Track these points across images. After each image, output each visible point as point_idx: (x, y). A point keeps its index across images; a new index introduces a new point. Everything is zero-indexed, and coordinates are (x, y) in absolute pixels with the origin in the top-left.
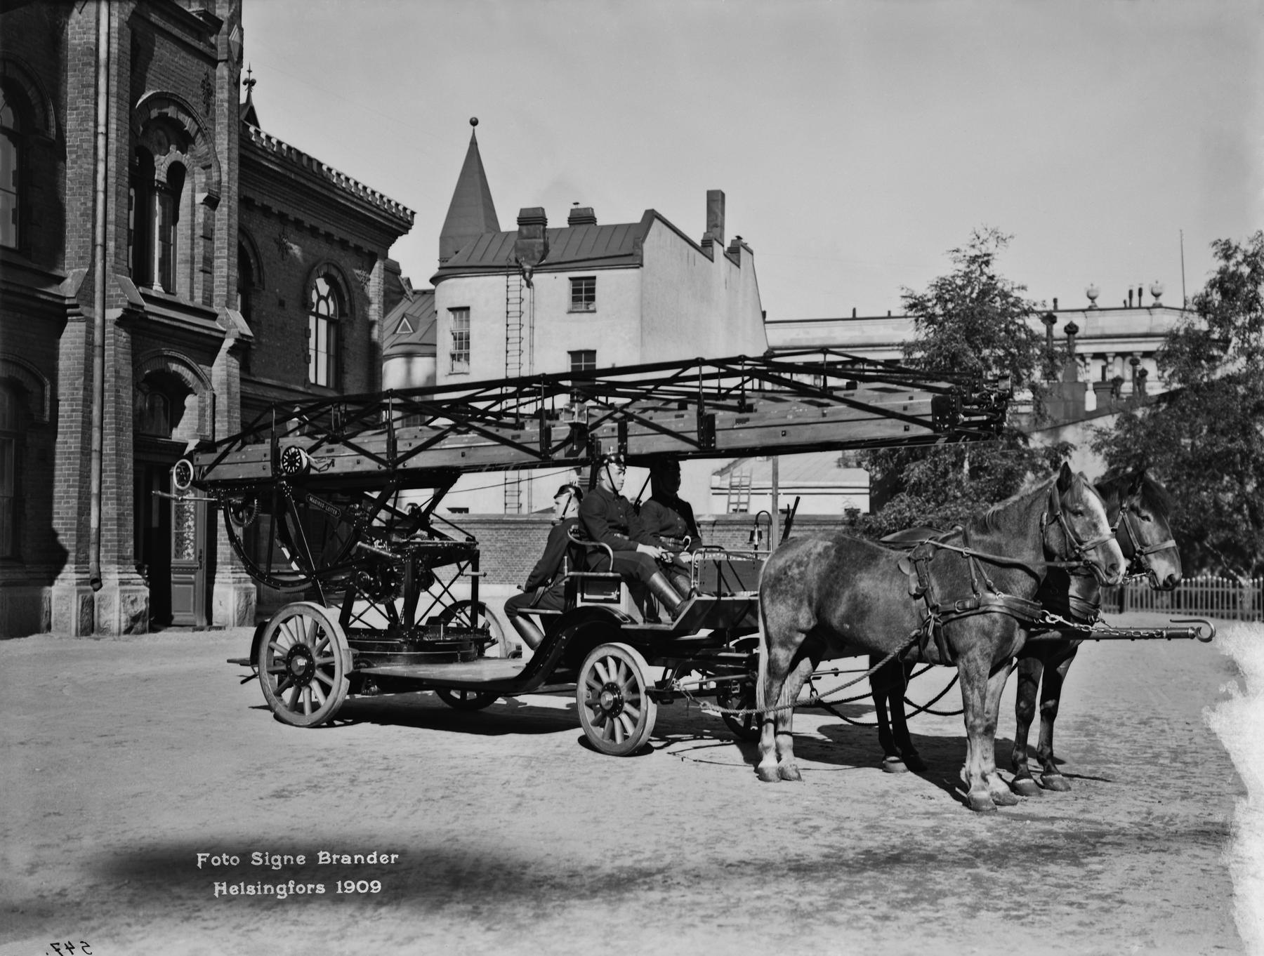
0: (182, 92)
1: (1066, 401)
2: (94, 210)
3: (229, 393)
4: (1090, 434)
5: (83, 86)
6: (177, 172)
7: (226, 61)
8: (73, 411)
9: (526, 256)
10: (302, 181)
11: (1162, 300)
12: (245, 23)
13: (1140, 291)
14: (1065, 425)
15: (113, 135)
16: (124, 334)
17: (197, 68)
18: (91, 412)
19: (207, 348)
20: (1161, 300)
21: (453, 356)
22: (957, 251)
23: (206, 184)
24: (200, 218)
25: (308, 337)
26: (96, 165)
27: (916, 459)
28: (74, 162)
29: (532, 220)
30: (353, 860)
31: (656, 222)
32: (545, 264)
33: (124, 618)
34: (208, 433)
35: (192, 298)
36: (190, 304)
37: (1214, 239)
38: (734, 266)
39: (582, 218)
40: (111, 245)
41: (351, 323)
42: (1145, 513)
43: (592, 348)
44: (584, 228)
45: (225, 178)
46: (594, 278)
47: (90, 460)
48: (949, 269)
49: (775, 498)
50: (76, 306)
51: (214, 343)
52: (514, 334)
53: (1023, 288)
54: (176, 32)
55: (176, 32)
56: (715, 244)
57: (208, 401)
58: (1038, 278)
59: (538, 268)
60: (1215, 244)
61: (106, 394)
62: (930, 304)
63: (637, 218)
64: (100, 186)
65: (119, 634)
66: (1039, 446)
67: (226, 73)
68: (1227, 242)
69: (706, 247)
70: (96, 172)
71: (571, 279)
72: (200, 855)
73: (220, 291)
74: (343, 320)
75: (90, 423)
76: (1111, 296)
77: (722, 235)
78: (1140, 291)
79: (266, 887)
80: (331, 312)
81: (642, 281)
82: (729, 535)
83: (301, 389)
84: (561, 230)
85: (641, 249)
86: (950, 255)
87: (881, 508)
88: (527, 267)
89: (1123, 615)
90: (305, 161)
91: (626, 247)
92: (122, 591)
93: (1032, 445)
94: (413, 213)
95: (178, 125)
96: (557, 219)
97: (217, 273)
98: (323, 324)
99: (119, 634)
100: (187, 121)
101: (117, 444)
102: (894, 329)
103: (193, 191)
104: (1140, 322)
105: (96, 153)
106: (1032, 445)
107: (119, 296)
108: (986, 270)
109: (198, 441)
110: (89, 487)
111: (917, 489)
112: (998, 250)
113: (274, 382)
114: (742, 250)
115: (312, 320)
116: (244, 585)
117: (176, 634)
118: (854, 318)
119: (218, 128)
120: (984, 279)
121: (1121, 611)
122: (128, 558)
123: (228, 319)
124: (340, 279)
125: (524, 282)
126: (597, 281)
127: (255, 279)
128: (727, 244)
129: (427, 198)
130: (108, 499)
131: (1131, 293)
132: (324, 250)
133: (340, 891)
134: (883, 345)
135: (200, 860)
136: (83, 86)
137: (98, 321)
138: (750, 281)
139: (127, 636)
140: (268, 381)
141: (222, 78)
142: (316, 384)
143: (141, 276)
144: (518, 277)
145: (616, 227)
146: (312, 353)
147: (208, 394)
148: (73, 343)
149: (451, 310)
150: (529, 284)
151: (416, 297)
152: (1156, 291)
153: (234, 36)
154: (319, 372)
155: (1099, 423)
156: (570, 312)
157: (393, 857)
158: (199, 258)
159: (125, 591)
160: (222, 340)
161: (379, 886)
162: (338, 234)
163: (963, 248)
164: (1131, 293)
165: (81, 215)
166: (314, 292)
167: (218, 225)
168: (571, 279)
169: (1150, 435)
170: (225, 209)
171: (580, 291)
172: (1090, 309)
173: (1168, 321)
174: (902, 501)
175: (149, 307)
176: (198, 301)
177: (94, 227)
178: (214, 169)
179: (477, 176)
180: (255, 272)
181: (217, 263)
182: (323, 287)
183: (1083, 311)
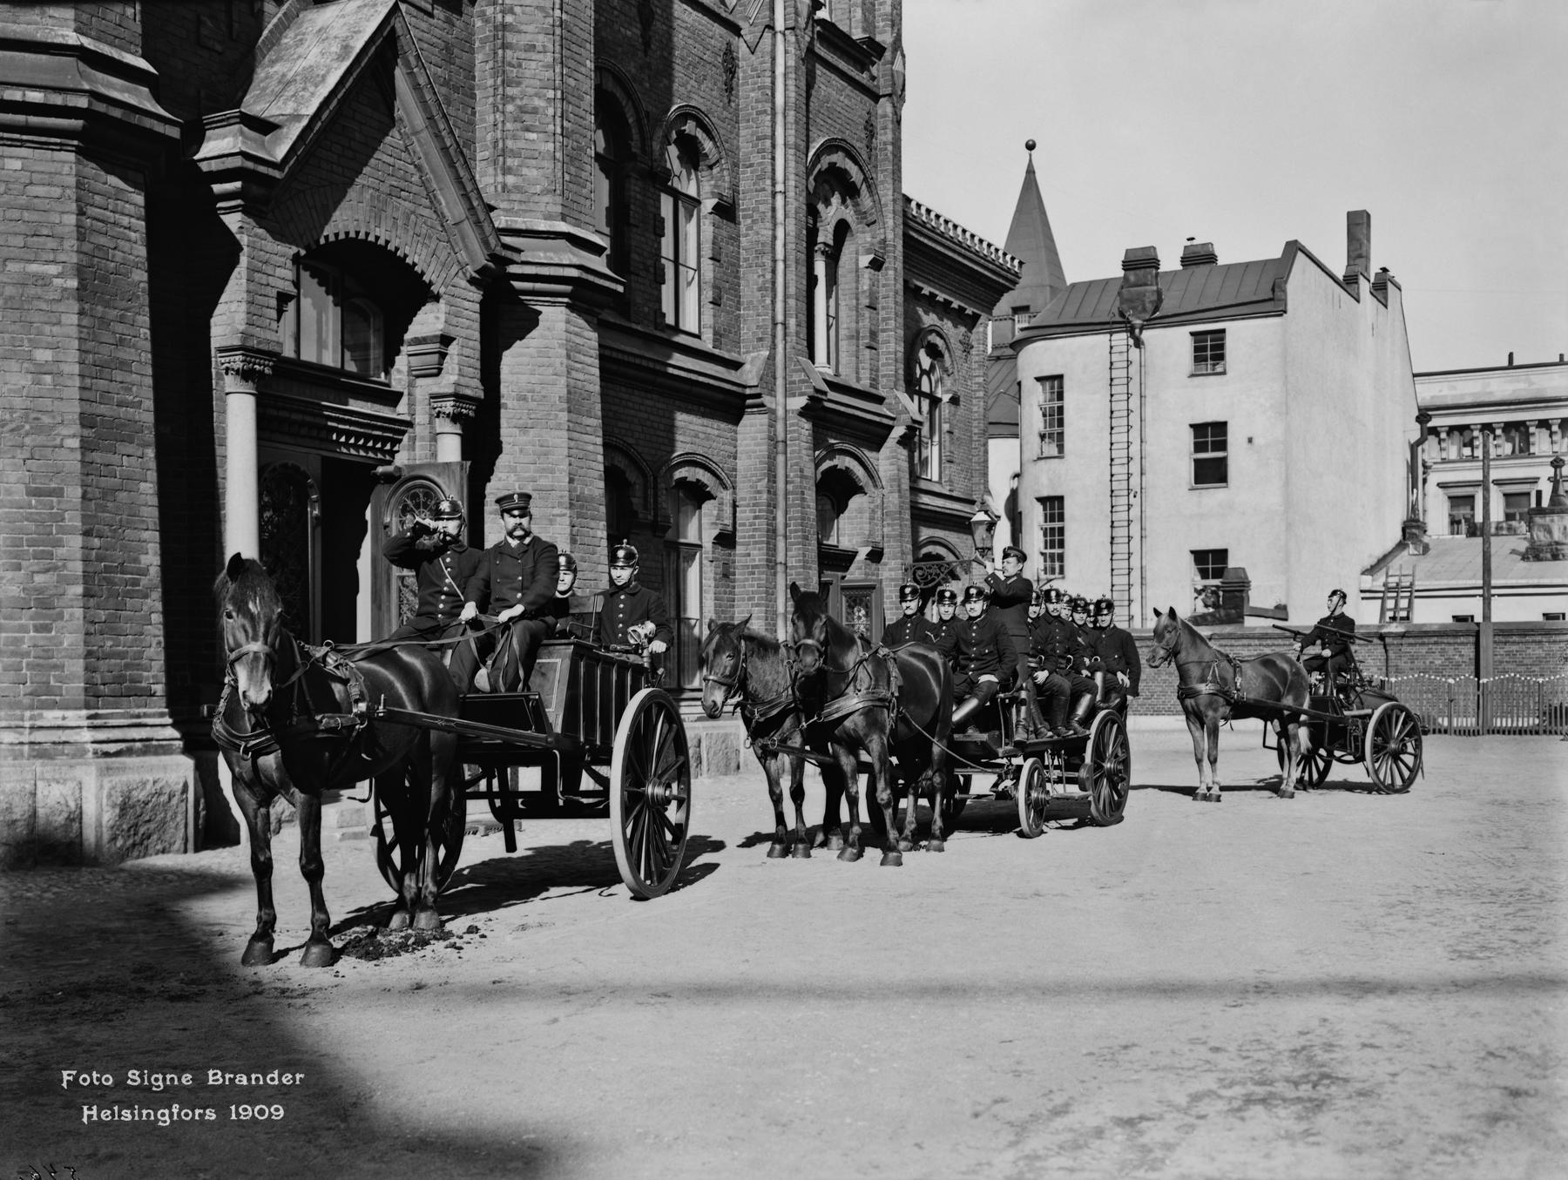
0: (847, 136)
2: (774, 283)
5: (758, 139)
6: (842, 229)
7: (890, 95)
8: (756, 518)
15: (791, 194)
17: (859, 102)
18: (775, 518)
21: (1042, 437)
26: (774, 230)
28: (750, 228)
29: (1140, 263)
30: (294, 1079)
35: (858, 379)
39: (1198, 258)
40: (792, 322)
43: (1221, 419)
44: (1204, 269)
45: (890, 236)
46: (1223, 331)
47: (775, 574)
50: (759, 396)
52: (1120, 406)
54: (842, 65)
55: (842, 65)
59: (1151, 323)
63: (1277, 253)
64: (780, 255)
67: (889, 109)
69: (1349, 282)
70: (774, 238)
71: (1192, 334)
72: (65, 1073)
75: (774, 531)
77: (1367, 268)
79: (145, 1112)
82: (1424, 650)
84: (1176, 272)
85: (1284, 291)
88: (1138, 322)
91: (1265, 290)
95: (844, 173)
96: (1170, 261)
97: (883, 349)
105: (774, 217)
110: (775, 606)
114: (1390, 285)
118: (1511, 366)
119: (881, 177)
125: (1131, 342)
133: (234, 1117)
135: (66, 1078)
136: (758, 139)
137: (780, 412)
138: (1399, 324)
141: (885, 116)
144: (1124, 335)
145: (1248, 265)
148: (754, 439)
149: (1038, 379)
150: (1138, 343)
156: (1192, 376)
157: (298, 1076)
158: (865, 333)
160: (891, 428)
161: (282, 1112)
165: (760, 290)
168: (1192, 334)
177: (773, 302)
181: (882, 336)
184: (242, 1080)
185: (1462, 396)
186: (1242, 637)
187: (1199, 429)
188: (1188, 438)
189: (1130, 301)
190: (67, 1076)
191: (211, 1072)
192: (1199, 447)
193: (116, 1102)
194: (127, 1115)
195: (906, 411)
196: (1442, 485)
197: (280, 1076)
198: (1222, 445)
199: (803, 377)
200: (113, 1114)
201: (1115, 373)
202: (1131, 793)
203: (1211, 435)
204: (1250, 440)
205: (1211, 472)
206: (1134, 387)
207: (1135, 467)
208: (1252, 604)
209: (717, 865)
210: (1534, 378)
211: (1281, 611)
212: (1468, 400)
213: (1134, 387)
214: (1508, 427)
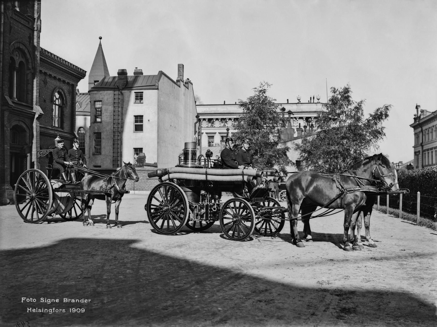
1: (288, 134)
4: (294, 146)
10: (52, 62)
12: (41, 18)
13: (314, 97)
20: (320, 101)
22: (256, 88)
29: (123, 73)
31: (163, 76)
38: (186, 89)
41: (66, 107)
42: (383, 166)
46: (143, 92)
48: (253, 94)
53: (275, 100)
63: (156, 73)
66: (280, 148)
68: (335, 89)
71: (135, 92)
72: (22, 298)
78: (314, 97)
83: (50, 128)
90: (53, 56)
91: (153, 83)
98: (57, 107)
104: (314, 107)
108: (264, 94)
114: (189, 83)
115: (54, 106)
118: (224, 104)
124: (62, 93)
126: (144, 93)
131: (311, 98)
132: (58, 84)
142: (55, 126)
145: (149, 76)
146: (54, 117)
150: (122, 94)
151: (81, 95)
152: (318, 98)
153: (39, 23)
155: (297, 141)
157: (89, 300)
160: (35, 115)
161: (84, 310)
162: (62, 78)
163: (257, 88)
164: (311, 98)
168: (135, 92)
172: (298, 103)
173: (319, 108)
182: (57, 96)
183: (296, 104)
184: (73, 301)
186: (143, 171)
187: (136, 117)
190: (23, 299)
192: (136, 121)
193: (54, 307)
194: (40, 311)
198: (142, 121)
202: (14, 206)
204: (149, 120)
205: (139, 128)
208: (146, 162)
209: (376, 246)
210: (228, 108)
211: (155, 165)
212: (213, 112)
214: (222, 119)
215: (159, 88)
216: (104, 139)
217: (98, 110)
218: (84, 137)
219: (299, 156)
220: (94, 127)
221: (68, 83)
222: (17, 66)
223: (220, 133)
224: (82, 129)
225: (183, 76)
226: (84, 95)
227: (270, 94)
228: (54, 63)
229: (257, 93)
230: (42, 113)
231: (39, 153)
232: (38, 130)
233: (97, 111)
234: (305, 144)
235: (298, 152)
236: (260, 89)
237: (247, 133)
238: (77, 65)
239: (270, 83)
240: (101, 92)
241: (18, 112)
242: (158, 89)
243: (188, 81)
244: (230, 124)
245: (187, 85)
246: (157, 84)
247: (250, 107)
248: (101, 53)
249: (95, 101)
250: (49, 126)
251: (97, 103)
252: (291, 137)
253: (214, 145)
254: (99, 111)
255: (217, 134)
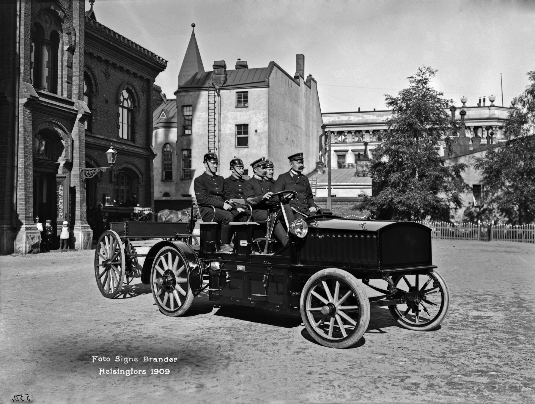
3: (79, 140)
4: (473, 161)
9: (217, 82)
10: (116, 45)
11: (495, 103)
13: (484, 99)
14: (461, 156)
16: (28, 111)
19: (69, 119)
20: (494, 103)
22: (412, 77)
23: (69, 41)
24: (66, 57)
25: (119, 117)
27: (394, 172)
29: (220, 66)
32: (225, 86)
33: (28, 246)
34: (70, 158)
35: (62, 95)
36: (61, 97)
37: (530, 71)
38: (308, 88)
39: (242, 66)
43: (246, 123)
45: (78, 39)
46: (247, 92)
48: (408, 85)
49: (330, 189)
51: (72, 116)
53: (442, 94)
56: (300, 78)
57: (70, 143)
58: (449, 89)
60: (529, 73)
61: (20, 139)
62: (399, 102)
63: (266, 65)
65: (26, 254)
71: (237, 92)
73: (75, 92)
74: (135, 109)
76: (472, 102)
78: (484, 99)
80: (129, 106)
81: (269, 93)
83: (115, 140)
84: (232, 71)
86: (408, 80)
87: (378, 194)
88: (217, 87)
89: (490, 242)
91: (262, 78)
92: (27, 233)
93: (446, 165)
94: (166, 62)
96: (231, 66)
97: (74, 83)
98: (126, 111)
99: (26, 254)
100: (60, 13)
101: (25, 163)
102: (377, 116)
103: (63, 44)
106: (446, 165)
107: (25, 92)
109: (65, 162)
111: (395, 185)
112: (430, 77)
113: (103, 137)
114: (312, 81)
115: (121, 109)
116: (87, 230)
117: (53, 253)
118: (359, 112)
119: (74, 16)
120: (424, 90)
121: (489, 240)
122: (30, 217)
123: (79, 105)
124: (133, 91)
125: (216, 94)
127: (94, 90)
128: (305, 78)
129: (172, 54)
130: (20, 189)
131: (480, 100)
134: (372, 123)
138: (315, 94)
139: (29, 255)
140: (100, 137)
142: (122, 138)
143: (38, 85)
144: (213, 92)
145: (257, 69)
146: (121, 124)
147: (70, 140)
151: (168, 102)
152: (492, 99)
154: (124, 133)
155: (478, 155)
156: (236, 107)
157: (175, 359)
159: (29, 233)
160: (76, 115)
161: (169, 371)
162: (132, 70)
164: (480, 100)
166: (122, 96)
167: (74, 61)
169: (502, 160)
170: (78, 53)
171: (241, 98)
174: (388, 190)
175: (41, 99)
176: (65, 96)
178: (72, 34)
179: (195, 50)
180: (94, 87)
181: (74, 78)
182: (126, 94)
184: (155, 360)
185: (342, 121)
187: (239, 126)
188: (234, 130)
189: (215, 80)
191: (145, 357)
192: (239, 133)
195: (82, 108)
196: (335, 151)
197: (169, 359)
198: (246, 133)
199: (26, 90)
200: (110, 372)
201: (210, 105)
203: (242, 128)
204: (256, 131)
206: (217, 111)
207: (217, 139)
210: (365, 116)
212: (344, 123)
213: (217, 111)
214: (356, 132)
215: (270, 85)
216: (195, 157)
217: (187, 118)
218: (171, 156)
219: (481, 177)
220: (182, 142)
221: (141, 77)
222: (47, 37)
223: (353, 151)
224: (168, 145)
225: (303, 71)
226: (173, 102)
227: (434, 85)
228: (119, 47)
229: (414, 85)
230: (89, 111)
231: (83, 172)
232: (82, 138)
233: (185, 119)
234: (492, 159)
235: (480, 171)
236: (420, 78)
237: (399, 143)
238: (153, 52)
239: (433, 69)
240: (191, 93)
241: (48, 109)
242: (268, 86)
243: (310, 78)
244: (367, 138)
245: (308, 84)
246: (267, 80)
247: (404, 105)
248: (194, 45)
249: (183, 106)
250: (114, 138)
251: (186, 109)
252: (465, 149)
253: (347, 166)
254: (188, 120)
255: (350, 151)
